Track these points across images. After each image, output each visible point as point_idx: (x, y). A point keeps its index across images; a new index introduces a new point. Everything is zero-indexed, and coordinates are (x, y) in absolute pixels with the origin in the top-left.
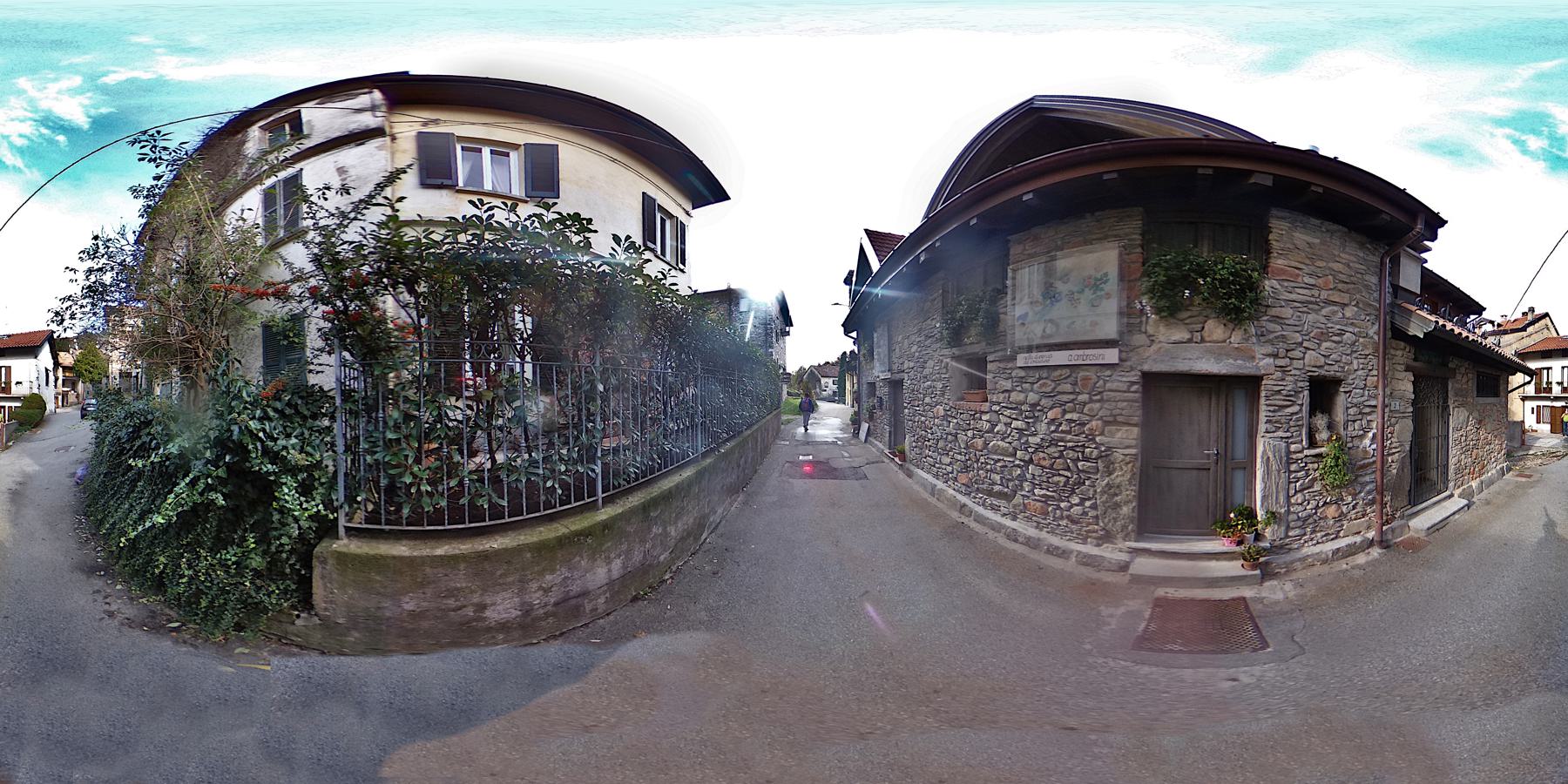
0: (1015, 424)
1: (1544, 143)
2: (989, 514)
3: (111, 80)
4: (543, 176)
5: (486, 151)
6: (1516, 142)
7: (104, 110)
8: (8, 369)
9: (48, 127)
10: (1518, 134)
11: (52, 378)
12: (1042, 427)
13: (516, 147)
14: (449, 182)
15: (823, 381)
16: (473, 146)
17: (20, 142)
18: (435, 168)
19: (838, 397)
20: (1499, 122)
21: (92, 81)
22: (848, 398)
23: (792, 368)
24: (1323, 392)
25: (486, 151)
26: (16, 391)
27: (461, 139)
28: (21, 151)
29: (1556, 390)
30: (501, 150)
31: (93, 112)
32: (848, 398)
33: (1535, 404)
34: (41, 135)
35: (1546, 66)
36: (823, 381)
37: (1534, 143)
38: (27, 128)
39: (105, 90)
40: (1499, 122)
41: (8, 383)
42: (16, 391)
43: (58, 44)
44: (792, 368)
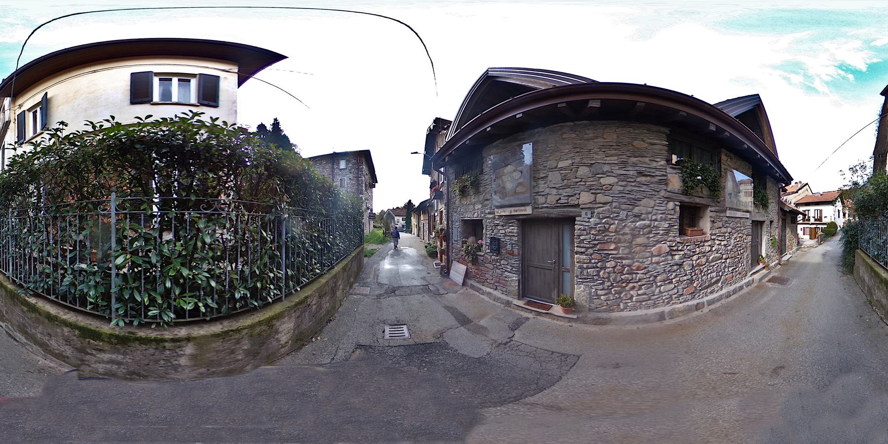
0: (723, 243)
1: (800, 79)
2: (715, 295)
3: (878, 43)
4: (209, 93)
5: (175, 80)
6: (785, 78)
7: (875, 60)
8: (821, 211)
9: (843, 70)
10: (785, 74)
11: (841, 214)
12: (732, 241)
13: (194, 76)
14: (147, 99)
15: (396, 218)
16: (166, 78)
17: (829, 79)
18: (140, 91)
19: (408, 228)
20: (774, 67)
21: (868, 44)
22: (415, 230)
23: (377, 210)
24: (771, 222)
25: (175, 80)
26: (824, 220)
27: (157, 74)
28: (827, 83)
29: (812, 220)
30: (184, 79)
31: (868, 62)
32: (415, 230)
33: (802, 226)
34: (839, 75)
35: (798, 35)
36: (396, 218)
37: (796, 79)
38: (833, 71)
39: (876, 49)
40: (774, 67)
41: (821, 217)
42: (824, 220)
43: (850, 24)
44: (377, 210)
